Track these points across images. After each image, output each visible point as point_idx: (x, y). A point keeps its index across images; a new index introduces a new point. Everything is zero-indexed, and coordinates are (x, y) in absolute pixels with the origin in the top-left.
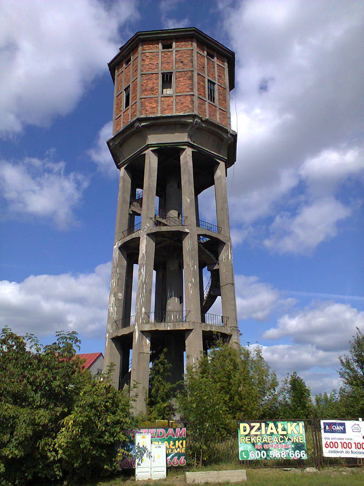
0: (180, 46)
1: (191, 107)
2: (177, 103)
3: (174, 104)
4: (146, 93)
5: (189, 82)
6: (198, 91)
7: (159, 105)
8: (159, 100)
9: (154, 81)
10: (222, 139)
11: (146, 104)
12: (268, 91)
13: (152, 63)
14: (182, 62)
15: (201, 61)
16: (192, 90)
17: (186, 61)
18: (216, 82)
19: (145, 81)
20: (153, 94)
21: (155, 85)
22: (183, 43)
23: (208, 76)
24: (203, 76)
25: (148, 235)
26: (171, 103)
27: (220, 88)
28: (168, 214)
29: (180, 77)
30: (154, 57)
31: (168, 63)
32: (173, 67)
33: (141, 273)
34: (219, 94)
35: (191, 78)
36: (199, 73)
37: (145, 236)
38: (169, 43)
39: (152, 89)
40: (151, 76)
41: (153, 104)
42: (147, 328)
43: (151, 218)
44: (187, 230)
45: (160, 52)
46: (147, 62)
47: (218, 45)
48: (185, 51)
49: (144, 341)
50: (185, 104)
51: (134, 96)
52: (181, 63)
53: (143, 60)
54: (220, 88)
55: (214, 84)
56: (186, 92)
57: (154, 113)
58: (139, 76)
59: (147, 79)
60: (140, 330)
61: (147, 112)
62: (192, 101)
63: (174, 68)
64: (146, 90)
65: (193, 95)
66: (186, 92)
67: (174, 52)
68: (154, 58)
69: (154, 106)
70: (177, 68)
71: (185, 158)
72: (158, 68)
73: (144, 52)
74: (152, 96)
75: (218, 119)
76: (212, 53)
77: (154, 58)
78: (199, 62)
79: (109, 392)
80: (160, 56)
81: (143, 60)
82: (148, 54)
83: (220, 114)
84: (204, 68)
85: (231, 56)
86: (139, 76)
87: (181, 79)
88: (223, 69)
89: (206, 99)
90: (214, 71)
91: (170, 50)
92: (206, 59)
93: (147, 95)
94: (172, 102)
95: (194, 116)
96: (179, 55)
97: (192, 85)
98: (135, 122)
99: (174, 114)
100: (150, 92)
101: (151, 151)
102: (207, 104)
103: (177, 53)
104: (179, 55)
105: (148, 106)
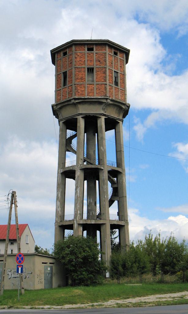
0: (98, 50)
1: (104, 92)
2: (97, 89)
3: (95, 89)
4: (78, 80)
5: (104, 75)
6: (109, 81)
7: (86, 89)
8: (86, 86)
9: (83, 73)
10: (121, 108)
11: (79, 88)
12: (146, 64)
13: (81, 60)
14: (99, 61)
15: (111, 59)
16: (105, 81)
17: (102, 61)
18: (119, 72)
19: (77, 73)
20: (82, 81)
21: (83, 75)
22: (100, 48)
23: (114, 69)
24: (111, 70)
25: (80, 169)
26: (93, 88)
27: (121, 75)
28: (97, 243)
29: (98, 72)
30: (82, 56)
31: (91, 61)
32: (95, 65)
33: (77, 192)
34: (121, 79)
35: (105, 73)
36: (109, 68)
37: (79, 170)
38: (91, 47)
39: (82, 79)
40: (81, 69)
41: (83, 89)
42: (81, 222)
43: (81, 159)
44: (102, 168)
45: (86, 53)
46: (78, 59)
47: (120, 47)
48: (101, 53)
49: (79, 229)
50: (101, 90)
51: (70, 80)
52: (98, 62)
53: (76, 58)
54: (121, 75)
55: (118, 73)
56: (102, 82)
57: (83, 94)
58: (74, 69)
59: (78, 71)
60: (78, 223)
61: (79, 94)
62: (106, 88)
63: (95, 65)
64: (78, 79)
65: (106, 84)
66: (102, 82)
67: (95, 53)
68: (82, 57)
69: (83, 90)
70: (97, 65)
71: (101, 123)
72: (85, 64)
73: (76, 52)
74: (82, 83)
75: (119, 98)
76: (117, 52)
77: (82, 57)
78: (110, 61)
79: (60, 69)
80: (86, 56)
81: (76, 58)
82: (79, 54)
83: (121, 92)
84: (112, 63)
85: (128, 52)
86: (74, 69)
87: (99, 73)
88: (123, 61)
89: (114, 85)
90: (118, 64)
91: (92, 52)
92: (113, 57)
93: (79, 82)
94: (94, 88)
95: (107, 99)
96: (97, 56)
97: (105, 77)
98: (72, 99)
99: (95, 97)
100: (80, 80)
101: (82, 117)
102: (114, 88)
103: (97, 54)
104: (97, 56)
105: (79, 90)
